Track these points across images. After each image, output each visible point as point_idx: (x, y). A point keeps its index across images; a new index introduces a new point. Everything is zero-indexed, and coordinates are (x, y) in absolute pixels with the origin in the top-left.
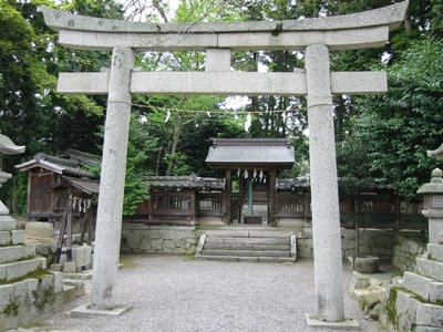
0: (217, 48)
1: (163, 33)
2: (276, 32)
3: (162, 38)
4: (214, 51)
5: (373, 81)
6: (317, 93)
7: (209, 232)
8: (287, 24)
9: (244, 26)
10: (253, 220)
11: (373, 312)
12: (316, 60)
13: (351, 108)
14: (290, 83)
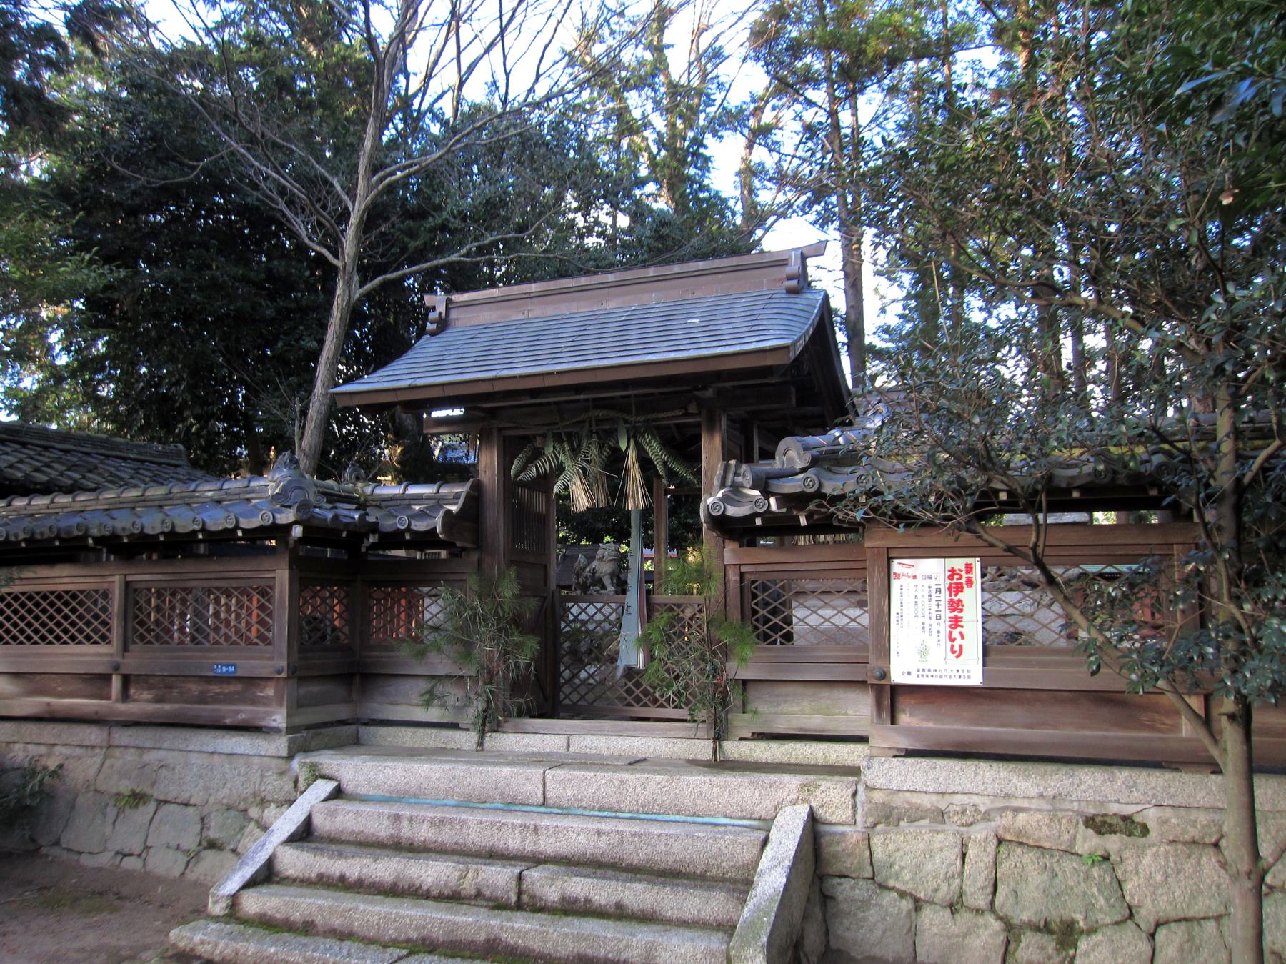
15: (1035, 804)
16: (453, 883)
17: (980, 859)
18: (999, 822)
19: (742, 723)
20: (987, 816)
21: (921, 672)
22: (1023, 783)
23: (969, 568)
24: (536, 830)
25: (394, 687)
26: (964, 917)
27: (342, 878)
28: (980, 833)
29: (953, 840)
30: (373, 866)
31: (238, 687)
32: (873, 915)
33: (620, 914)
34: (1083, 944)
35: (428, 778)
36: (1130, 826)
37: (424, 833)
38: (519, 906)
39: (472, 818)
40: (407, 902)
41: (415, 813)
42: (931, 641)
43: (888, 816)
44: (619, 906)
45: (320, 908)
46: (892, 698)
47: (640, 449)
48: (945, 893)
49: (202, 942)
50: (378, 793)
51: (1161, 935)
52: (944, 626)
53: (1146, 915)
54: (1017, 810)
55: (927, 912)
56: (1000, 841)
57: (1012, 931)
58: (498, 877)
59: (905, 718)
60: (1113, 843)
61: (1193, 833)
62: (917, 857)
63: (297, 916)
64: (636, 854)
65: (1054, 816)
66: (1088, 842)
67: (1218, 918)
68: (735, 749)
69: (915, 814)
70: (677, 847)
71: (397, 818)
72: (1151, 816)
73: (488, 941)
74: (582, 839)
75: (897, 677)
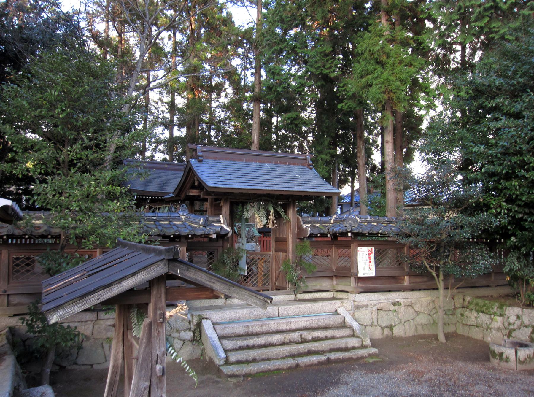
15: (384, 301)
16: (282, 340)
18: (378, 306)
20: (375, 305)
21: (364, 274)
23: (372, 249)
24: (290, 323)
26: (374, 327)
27: (247, 346)
28: (375, 309)
29: (370, 311)
30: (257, 340)
34: (394, 329)
35: (243, 314)
36: (399, 304)
37: (256, 329)
38: (302, 342)
39: (271, 322)
40: (272, 348)
41: (253, 324)
42: (366, 266)
44: (326, 337)
45: (258, 354)
47: (275, 210)
48: (370, 323)
49: (237, 371)
50: (224, 321)
51: (405, 324)
52: (368, 262)
53: (403, 321)
54: (381, 303)
55: (367, 327)
56: (378, 310)
57: (383, 329)
60: (396, 307)
61: (408, 304)
63: (250, 358)
64: (316, 325)
66: (393, 308)
67: (413, 319)
69: (363, 306)
70: (326, 321)
71: (248, 326)
72: (402, 301)
73: (308, 351)
74: (303, 323)
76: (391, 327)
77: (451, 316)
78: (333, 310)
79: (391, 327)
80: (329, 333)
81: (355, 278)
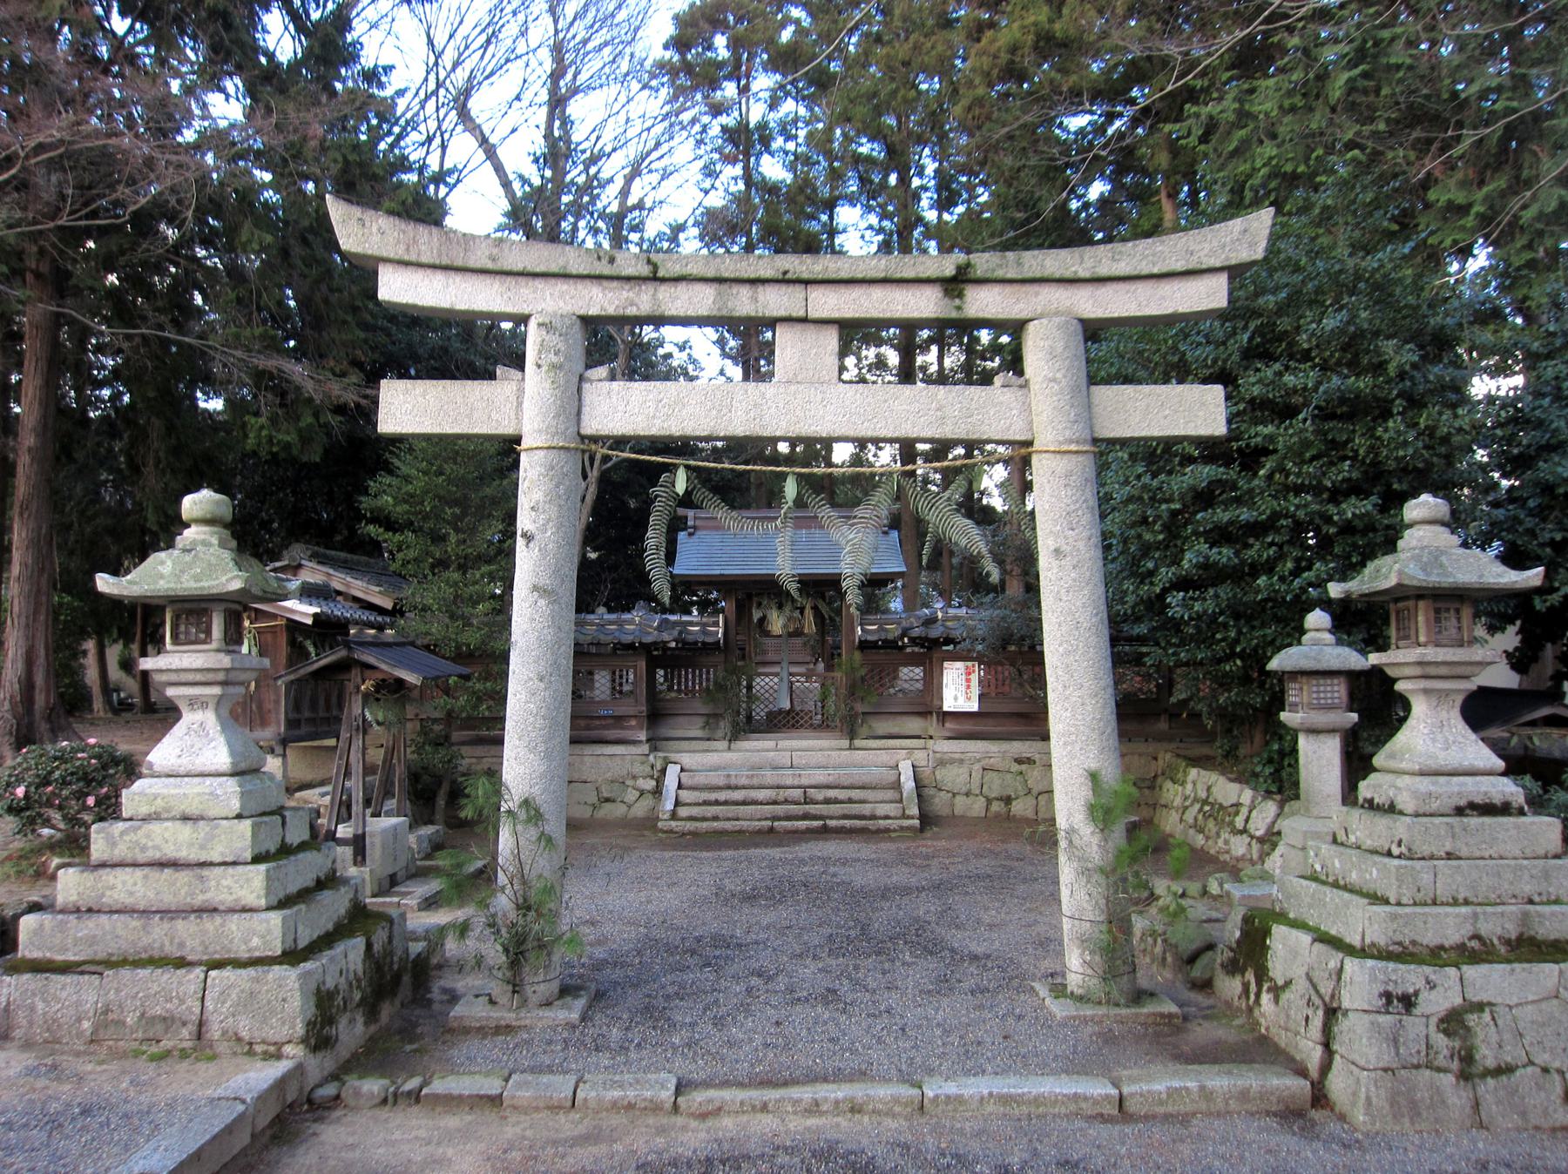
0: (804, 320)
1: (663, 280)
2: (954, 284)
3: (665, 292)
4: (799, 327)
5: (1198, 411)
6: (1045, 411)
7: (687, 759)
8: (983, 262)
9: (881, 266)
10: (781, 722)
11: (1197, 972)
12: (1047, 355)
13: (908, 33)
14: (987, 412)
17: (976, 776)
18: (984, 763)
19: (864, 731)
22: (993, 747)
25: (671, 721)
28: (977, 767)
31: (610, 721)
32: (937, 800)
33: (850, 801)
43: (941, 763)
46: (946, 716)
48: (964, 790)
53: (1035, 792)
57: (989, 801)
58: (797, 793)
59: (948, 725)
60: (1024, 767)
62: (954, 777)
65: (1003, 758)
66: (1015, 767)
68: (857, 743)
69: (952, 762)
72: (1037, 757)
75: (946, 708)
76: (1008, 800)
77: (1146, 791)
78: (892, 763)
79: (1008, 800)
80: (856, 794)
81: (938, 714)
